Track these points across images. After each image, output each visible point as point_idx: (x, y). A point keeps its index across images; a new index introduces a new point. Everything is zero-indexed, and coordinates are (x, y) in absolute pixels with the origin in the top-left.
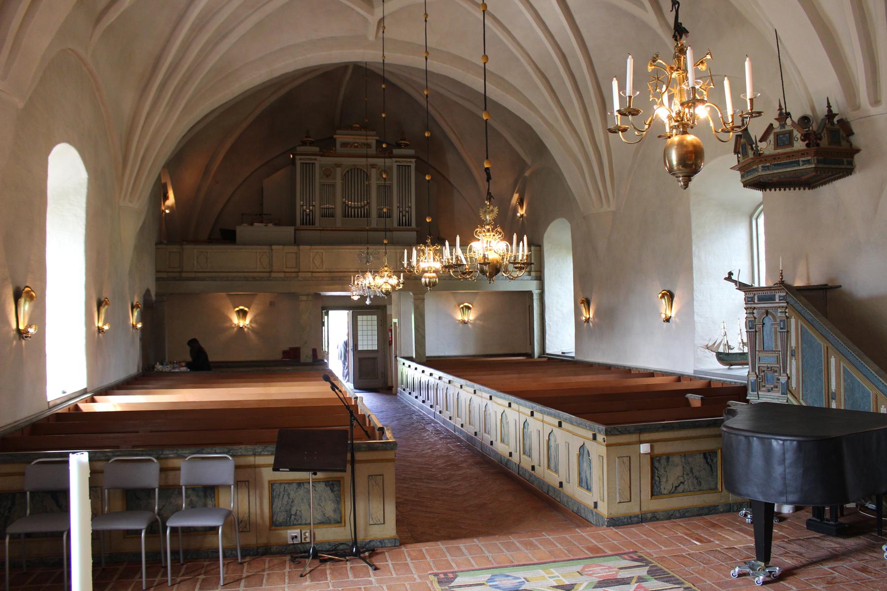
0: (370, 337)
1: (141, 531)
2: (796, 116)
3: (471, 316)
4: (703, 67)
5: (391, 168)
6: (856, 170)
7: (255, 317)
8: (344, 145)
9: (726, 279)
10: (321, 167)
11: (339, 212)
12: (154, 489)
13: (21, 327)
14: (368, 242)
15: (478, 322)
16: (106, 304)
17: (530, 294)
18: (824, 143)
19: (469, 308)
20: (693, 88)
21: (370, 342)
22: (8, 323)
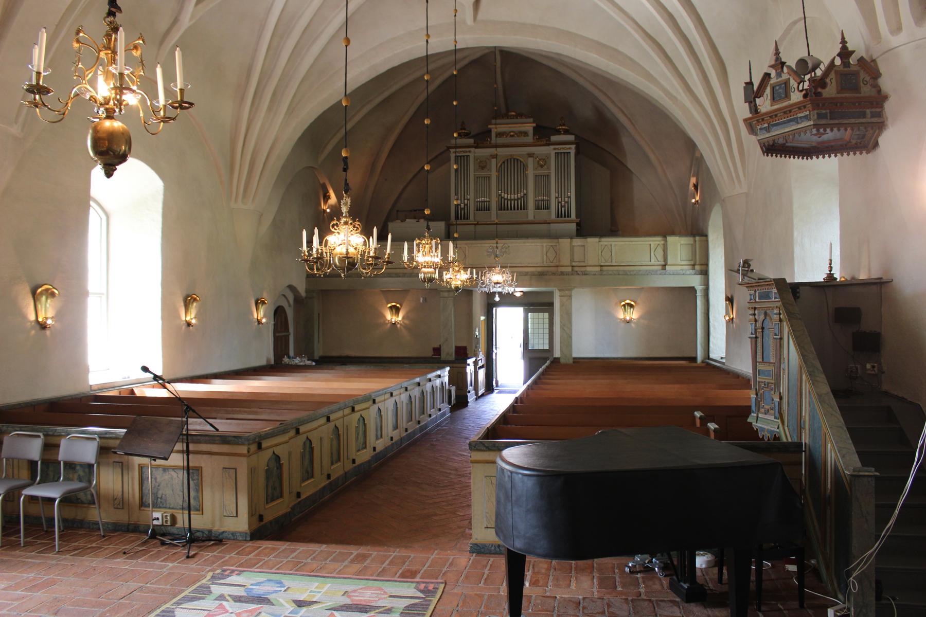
0: (541, 336)
1: (54, 500)
2: (792, 62)
3: (633, 314)
4: (136, 53)
5: (548, 156)
6: (889, 122)
7: (407, 313)
8: (499, 135)
10: (476, 159)
11: (494, 206)
12: (37, 462)
13: (40, 320)
14: (497, 236)
15: (642, 321)
16: (195, 300)
17: (692, 290)
18: (830, 91)
19: (631, 306)
20: (121, 75)
21: (541, 341)
22: (24, 317)
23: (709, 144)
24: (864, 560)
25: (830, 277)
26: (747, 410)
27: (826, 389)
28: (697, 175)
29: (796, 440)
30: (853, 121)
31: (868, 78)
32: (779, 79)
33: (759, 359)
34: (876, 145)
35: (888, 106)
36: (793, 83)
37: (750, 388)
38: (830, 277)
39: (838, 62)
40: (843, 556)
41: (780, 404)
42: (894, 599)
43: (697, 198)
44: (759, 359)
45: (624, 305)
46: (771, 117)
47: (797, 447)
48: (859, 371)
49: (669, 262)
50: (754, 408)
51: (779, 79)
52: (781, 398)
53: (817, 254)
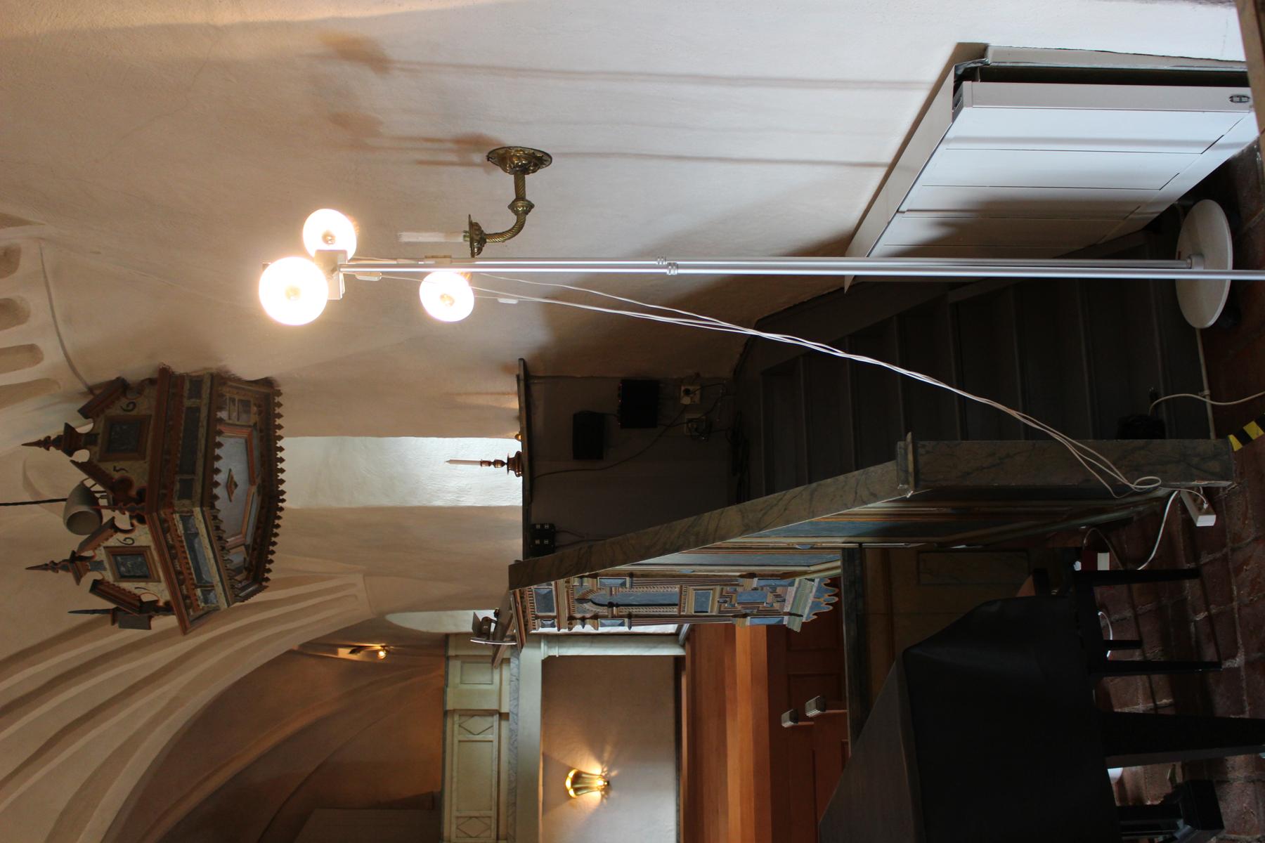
6: (213, 365)
9: (537, 160)
15: (606, 756)
17: (548, 663)
18: (137, 472)
23: (266, 641)
24: (1086, 457)
25: (514, 464)
26: (777, 634)
27: (732, 514)
28: (334, 648)
29: (839, 555)
30: (202, 432)
31: (124, 402)
32: (107, 565)
33: (675, 611)
34: (267, 382)
35: (181, 365)
36: (116, 540)
37: (733, 626)
38: (514, 464)
39: (83, 455)
40: (1088, 495)
41: (762, 576)
42: (1155, 396)
43: (377, 647)
44: (675, 611)
45: (576, 790)
46: (181, 583)
47: (851, 556)
48: (698, 416)
49: (495, 707)
50: (773, 621)
51: (107, 565)
52: (751, 575)
53: (471, 473)
